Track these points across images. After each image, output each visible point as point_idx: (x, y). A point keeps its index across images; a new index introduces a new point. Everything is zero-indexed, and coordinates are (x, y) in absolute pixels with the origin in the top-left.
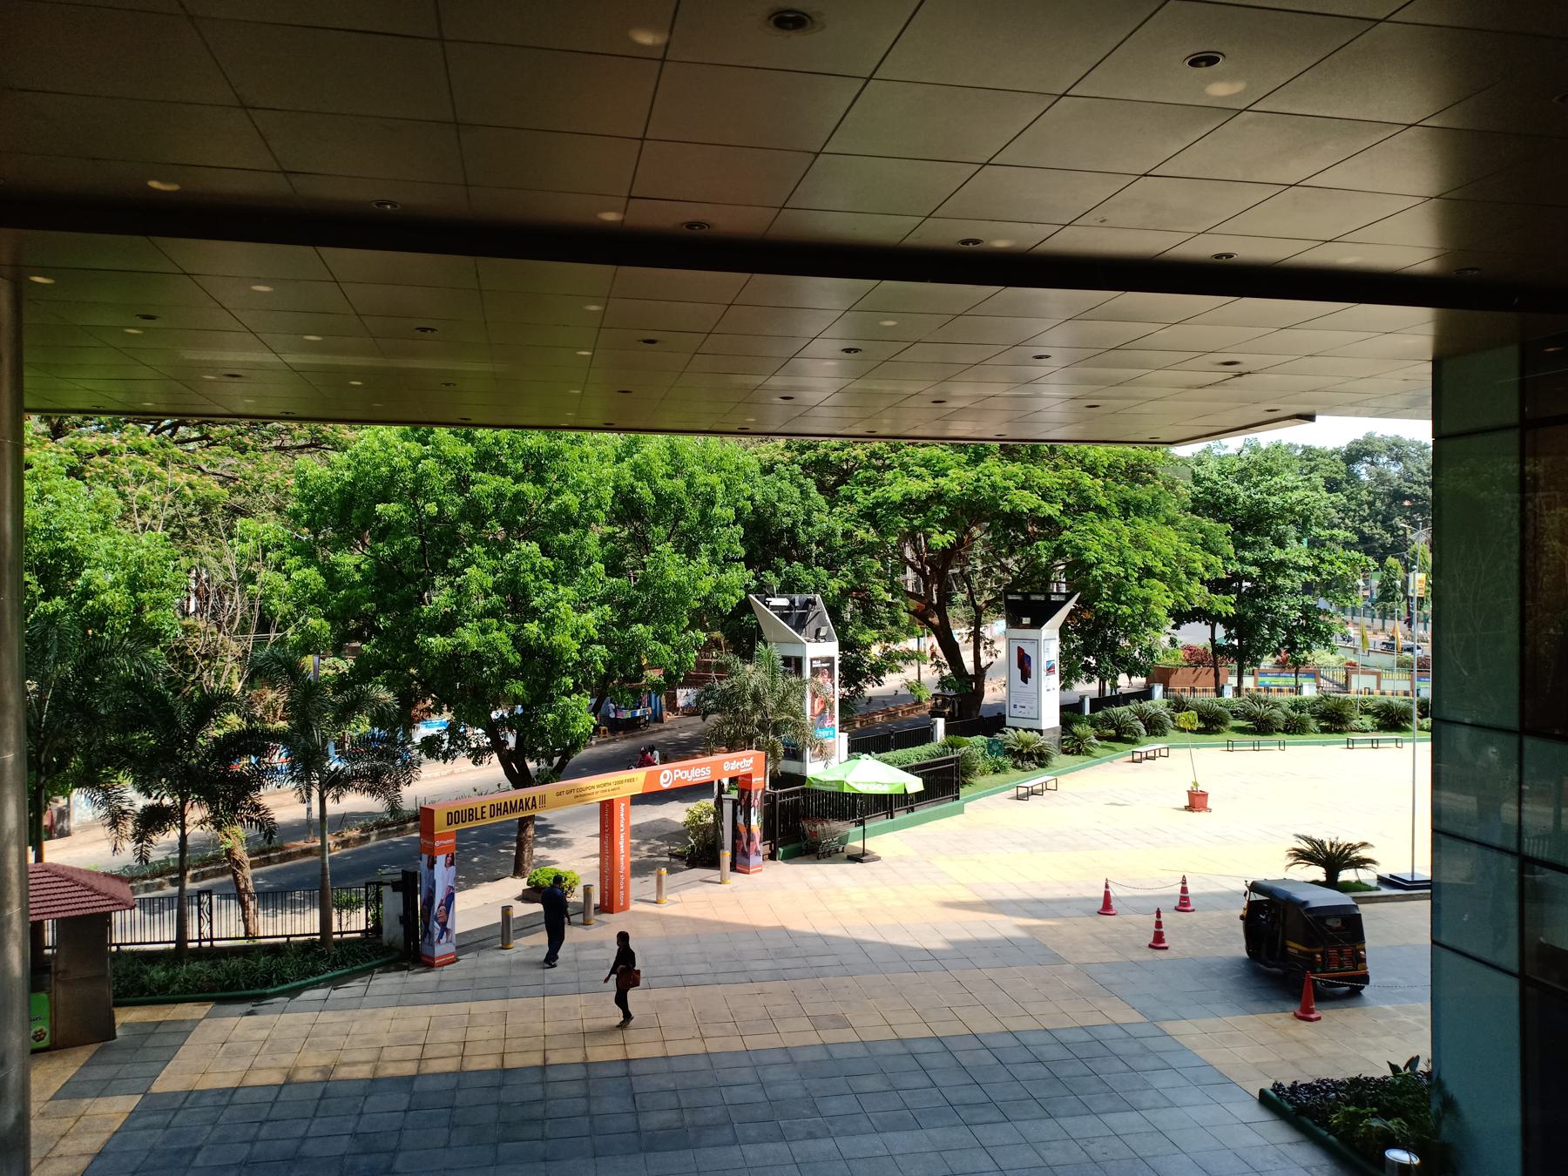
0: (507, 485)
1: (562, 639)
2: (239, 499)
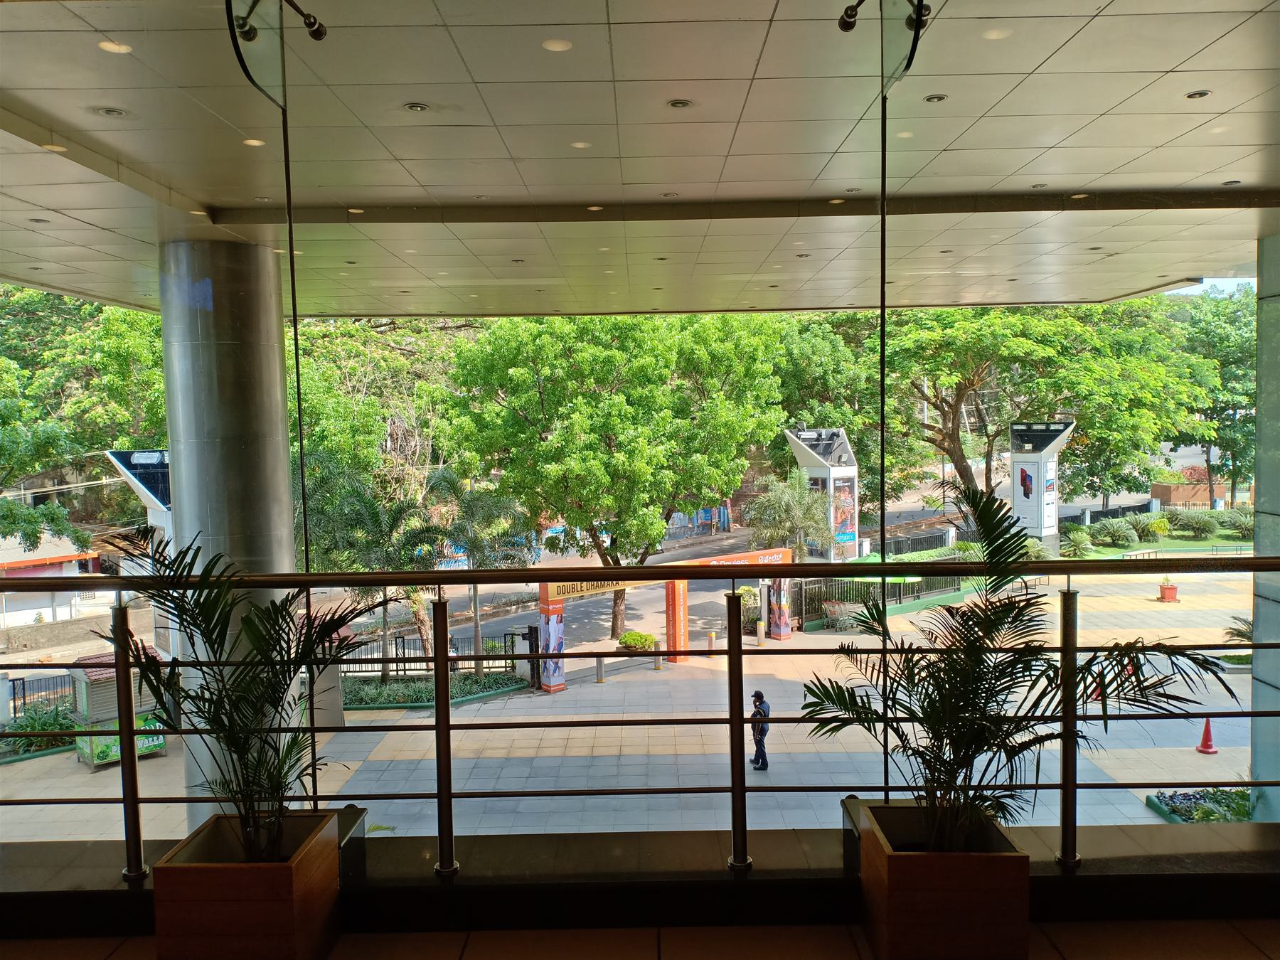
0: (602, 353)
1: (640, 465)
2: (419, 366)
